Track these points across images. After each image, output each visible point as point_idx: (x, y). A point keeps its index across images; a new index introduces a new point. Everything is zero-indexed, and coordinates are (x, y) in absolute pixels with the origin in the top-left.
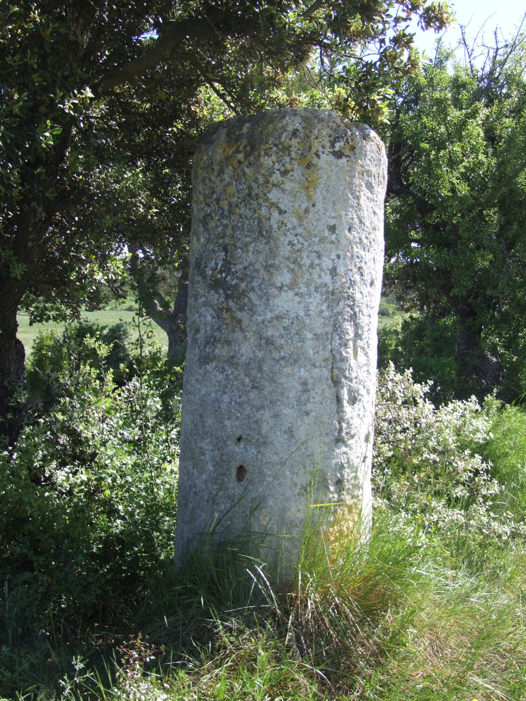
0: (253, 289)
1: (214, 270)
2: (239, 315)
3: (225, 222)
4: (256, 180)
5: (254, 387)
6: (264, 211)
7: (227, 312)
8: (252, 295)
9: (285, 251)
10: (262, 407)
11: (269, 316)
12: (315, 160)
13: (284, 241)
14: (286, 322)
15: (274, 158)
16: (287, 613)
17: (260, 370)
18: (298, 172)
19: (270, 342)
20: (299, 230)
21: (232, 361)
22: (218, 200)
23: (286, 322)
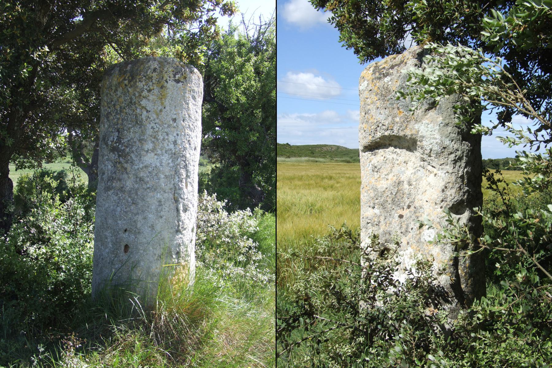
0: (133, 152)
1: (112, 142)
2: (125, 165)
3: (118, 116)
4: (134, 95)
5: (133, 203)
6: (138, 111)
8: (132, 155)
9: (149, 132)
10: (138, 214)
15: (144, 83)
17: (137, 194)
18: (156, 91)
19: (141, 179)
20: (157, 121)
21: (122, 190)
22: (114, 105)
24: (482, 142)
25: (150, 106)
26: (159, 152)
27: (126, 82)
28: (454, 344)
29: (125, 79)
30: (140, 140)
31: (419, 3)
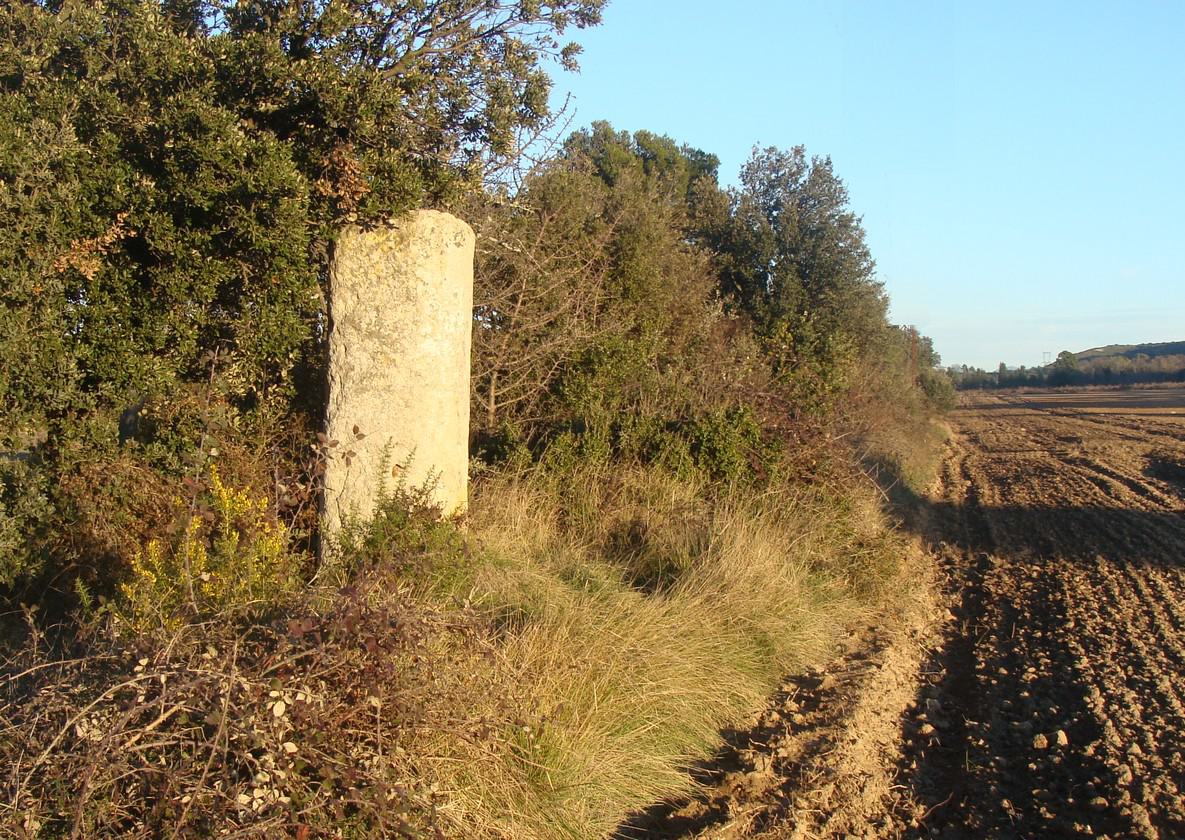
0: (404, 337)
1: (368, 325)
2: (392, 356)
3: (374, 289)
4: (406, 262)
5: (407, 406)
6: (411, 283)
7: (303, 806)
8: (403, 341)
9: (427, 311)
10: (413, 420)
11: (418, 355)
12: (445, 249)
13: (427, 303)
14: (429, 360)
15: (419, 247)
16: (70, 695)
17: (411, 393)
18: (435, 256)
19: (418, 375)
20: (436, 297)
21: (388, 389)
22: (366, 273)
23: (429, 360)
24: (1169, 341)
25: (427, 277)
26: (439, 337)
27: (392, 244)
28: (285, 483)
29: (388, 239)
30: (415, 322)
31: (1132, 800)
